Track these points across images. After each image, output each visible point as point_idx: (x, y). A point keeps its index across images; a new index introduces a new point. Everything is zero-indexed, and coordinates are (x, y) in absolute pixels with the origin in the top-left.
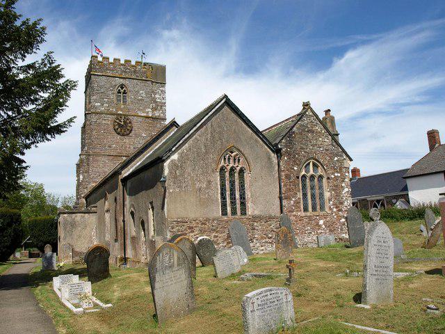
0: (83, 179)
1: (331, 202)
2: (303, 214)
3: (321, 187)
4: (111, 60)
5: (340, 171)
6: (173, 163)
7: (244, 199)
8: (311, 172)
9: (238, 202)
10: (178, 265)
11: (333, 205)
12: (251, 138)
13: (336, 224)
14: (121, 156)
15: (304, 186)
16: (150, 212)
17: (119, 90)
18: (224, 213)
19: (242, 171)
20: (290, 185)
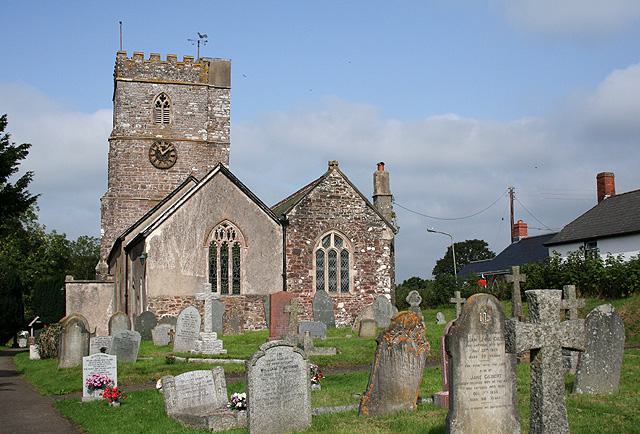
6: (156, 241)
15: (320, 264)
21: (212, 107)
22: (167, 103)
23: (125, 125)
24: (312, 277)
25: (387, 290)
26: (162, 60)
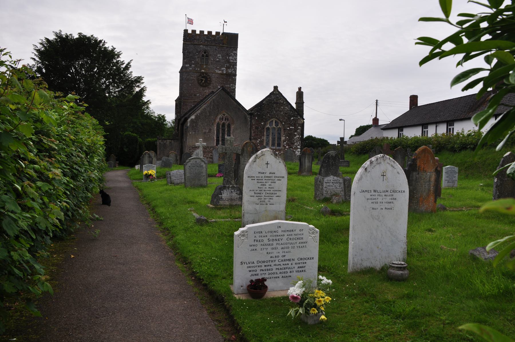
1: (285, 143)
5: (295, 125)
11: (286, 144)
17: (203, 55)
21: (229, 57)
22: (207, 55)
24: (263, 140)
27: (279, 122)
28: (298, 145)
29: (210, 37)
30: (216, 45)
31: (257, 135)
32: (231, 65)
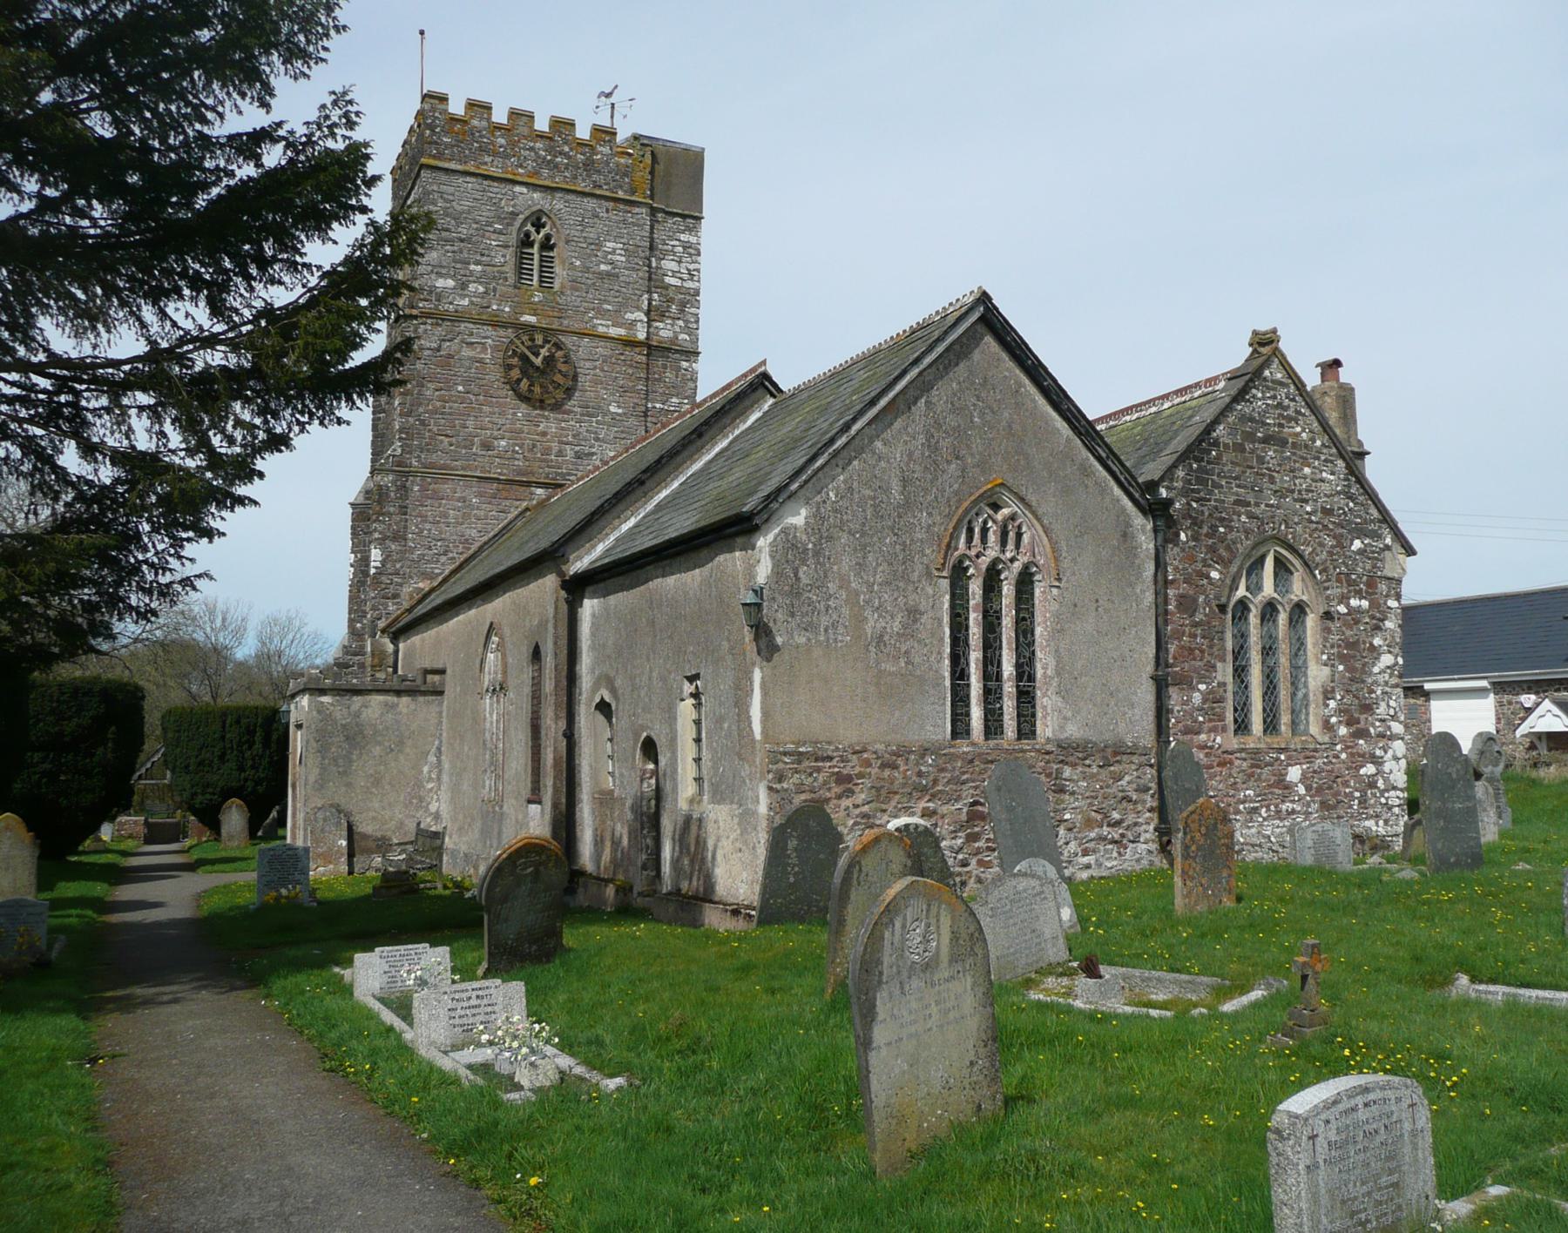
0: (383, 562)
1: (1332, 704)
2: (1234, 743)
3: (1299, 645)
4: (500, 116)
5: (1370, 590)
7: (1031, 678)
8: (1268, 588)
9: (1009, 688)
10: (954, 959)
12: (1085, 471)
13: (1346, 784)
14: (528, 484)
16: (686, 708)
17: (527, 235)
18: (960, 726)
19: (1025, 582)
20: (1194, 636)
22: (548, 237)
23: (440, 283)
24: (1223, 685)
25: (1397, 728)
26: (538, 126)
27: (1296, 562)
28: (1394, 718)
29: (566, 149)
30: (598, 192)
31: (1191, 650)
32: (671, 300)
